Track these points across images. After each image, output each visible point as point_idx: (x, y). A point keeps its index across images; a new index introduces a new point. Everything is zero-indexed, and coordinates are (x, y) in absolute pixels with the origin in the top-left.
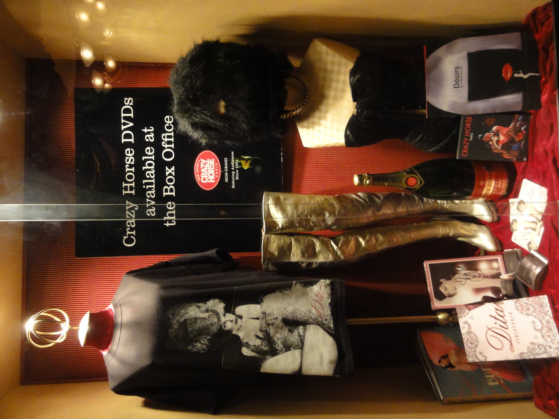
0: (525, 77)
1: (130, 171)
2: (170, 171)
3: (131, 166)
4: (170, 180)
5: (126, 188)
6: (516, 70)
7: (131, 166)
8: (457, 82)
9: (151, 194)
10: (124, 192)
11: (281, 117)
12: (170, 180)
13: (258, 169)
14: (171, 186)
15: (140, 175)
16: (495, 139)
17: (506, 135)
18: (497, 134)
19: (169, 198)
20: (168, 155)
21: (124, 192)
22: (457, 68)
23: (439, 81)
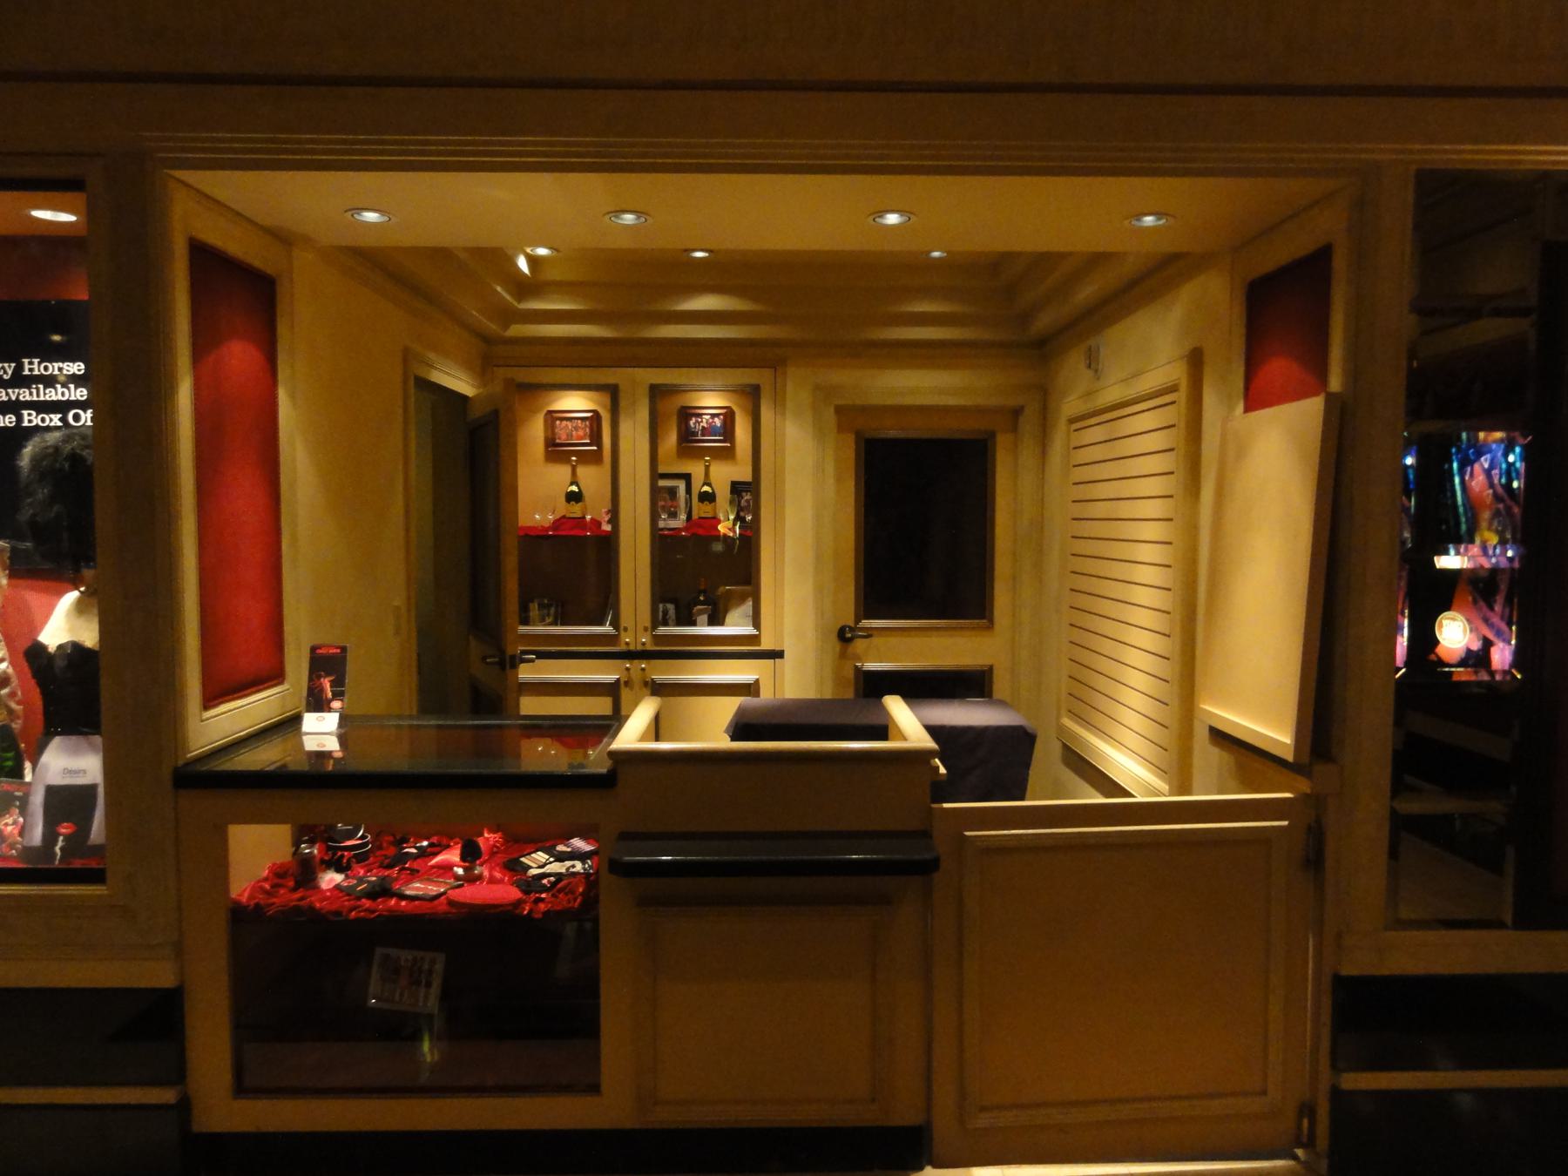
0: (57, 849)
1: (53, 368)
2: (55, 420)
3: (60, 369)
4: (43, 420)
5: (31, 363)
6: (67, 838)
7: (60, 369)
8: (70, 772)
9: (25, 395)
10: (26, 361)
11: (1502, 656)
12: (43, 420)
13: (718, 547)
14: (37, 421)
15: (49, 381)
16: (10, 821)
17: (11, 833)
18: (15, 823)
19: (20, 419)
20: (77, 418)
21: (26, 361)
22: (85, 772)
23: (75, 752)
